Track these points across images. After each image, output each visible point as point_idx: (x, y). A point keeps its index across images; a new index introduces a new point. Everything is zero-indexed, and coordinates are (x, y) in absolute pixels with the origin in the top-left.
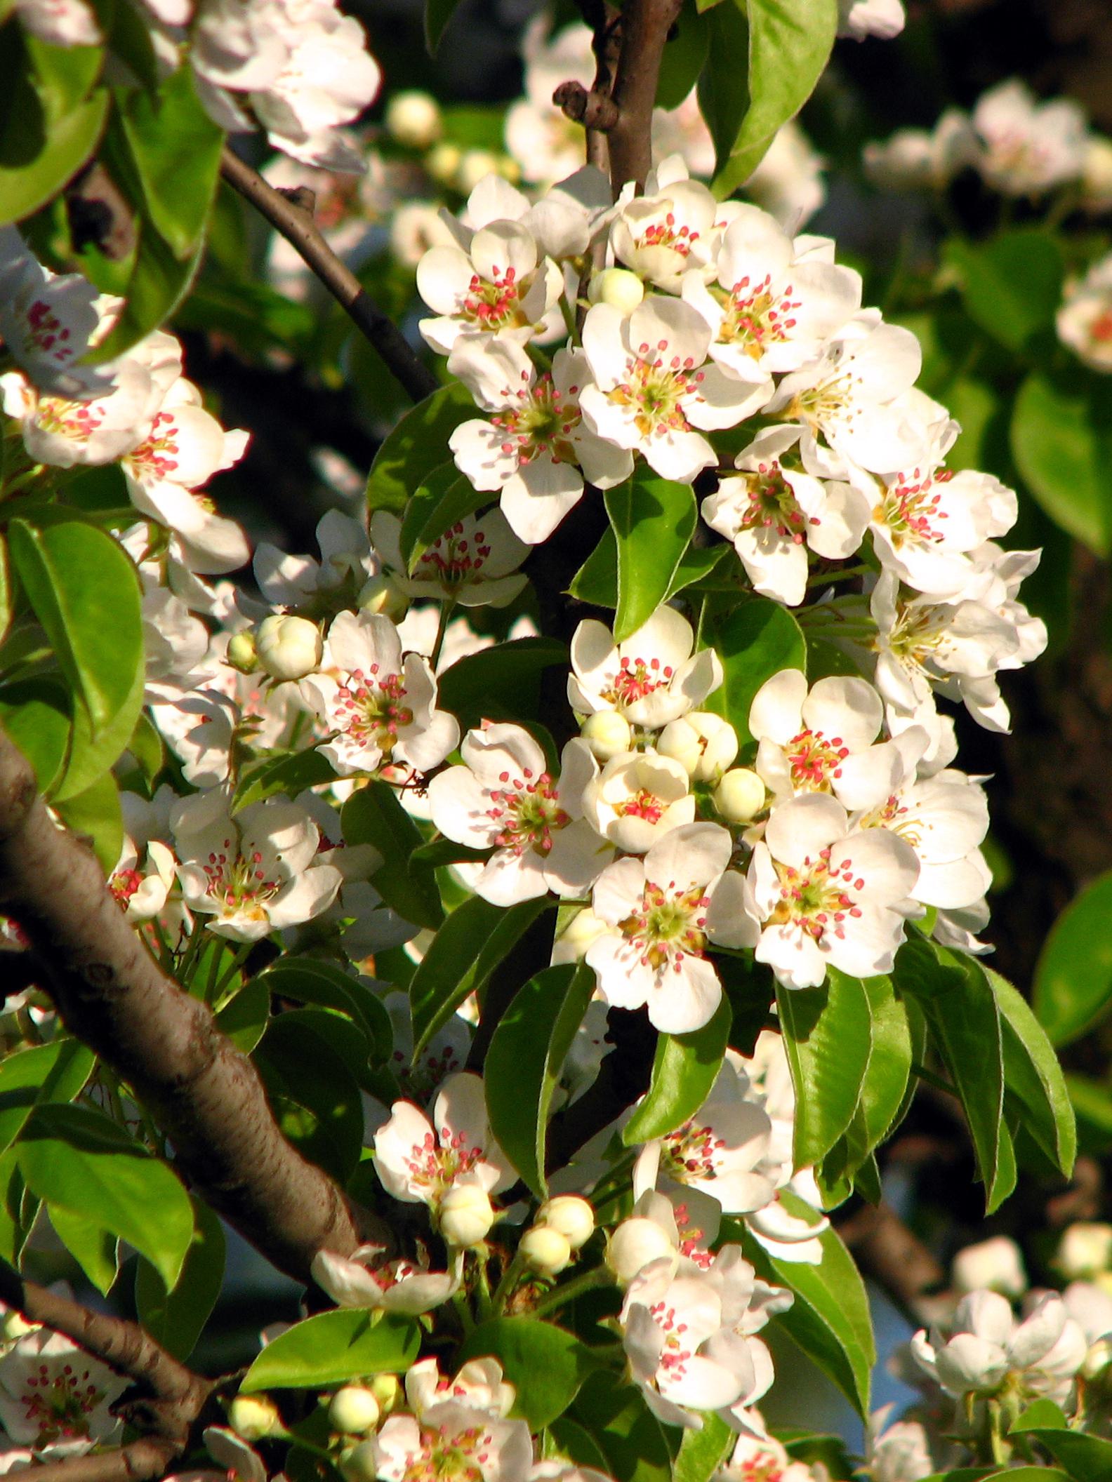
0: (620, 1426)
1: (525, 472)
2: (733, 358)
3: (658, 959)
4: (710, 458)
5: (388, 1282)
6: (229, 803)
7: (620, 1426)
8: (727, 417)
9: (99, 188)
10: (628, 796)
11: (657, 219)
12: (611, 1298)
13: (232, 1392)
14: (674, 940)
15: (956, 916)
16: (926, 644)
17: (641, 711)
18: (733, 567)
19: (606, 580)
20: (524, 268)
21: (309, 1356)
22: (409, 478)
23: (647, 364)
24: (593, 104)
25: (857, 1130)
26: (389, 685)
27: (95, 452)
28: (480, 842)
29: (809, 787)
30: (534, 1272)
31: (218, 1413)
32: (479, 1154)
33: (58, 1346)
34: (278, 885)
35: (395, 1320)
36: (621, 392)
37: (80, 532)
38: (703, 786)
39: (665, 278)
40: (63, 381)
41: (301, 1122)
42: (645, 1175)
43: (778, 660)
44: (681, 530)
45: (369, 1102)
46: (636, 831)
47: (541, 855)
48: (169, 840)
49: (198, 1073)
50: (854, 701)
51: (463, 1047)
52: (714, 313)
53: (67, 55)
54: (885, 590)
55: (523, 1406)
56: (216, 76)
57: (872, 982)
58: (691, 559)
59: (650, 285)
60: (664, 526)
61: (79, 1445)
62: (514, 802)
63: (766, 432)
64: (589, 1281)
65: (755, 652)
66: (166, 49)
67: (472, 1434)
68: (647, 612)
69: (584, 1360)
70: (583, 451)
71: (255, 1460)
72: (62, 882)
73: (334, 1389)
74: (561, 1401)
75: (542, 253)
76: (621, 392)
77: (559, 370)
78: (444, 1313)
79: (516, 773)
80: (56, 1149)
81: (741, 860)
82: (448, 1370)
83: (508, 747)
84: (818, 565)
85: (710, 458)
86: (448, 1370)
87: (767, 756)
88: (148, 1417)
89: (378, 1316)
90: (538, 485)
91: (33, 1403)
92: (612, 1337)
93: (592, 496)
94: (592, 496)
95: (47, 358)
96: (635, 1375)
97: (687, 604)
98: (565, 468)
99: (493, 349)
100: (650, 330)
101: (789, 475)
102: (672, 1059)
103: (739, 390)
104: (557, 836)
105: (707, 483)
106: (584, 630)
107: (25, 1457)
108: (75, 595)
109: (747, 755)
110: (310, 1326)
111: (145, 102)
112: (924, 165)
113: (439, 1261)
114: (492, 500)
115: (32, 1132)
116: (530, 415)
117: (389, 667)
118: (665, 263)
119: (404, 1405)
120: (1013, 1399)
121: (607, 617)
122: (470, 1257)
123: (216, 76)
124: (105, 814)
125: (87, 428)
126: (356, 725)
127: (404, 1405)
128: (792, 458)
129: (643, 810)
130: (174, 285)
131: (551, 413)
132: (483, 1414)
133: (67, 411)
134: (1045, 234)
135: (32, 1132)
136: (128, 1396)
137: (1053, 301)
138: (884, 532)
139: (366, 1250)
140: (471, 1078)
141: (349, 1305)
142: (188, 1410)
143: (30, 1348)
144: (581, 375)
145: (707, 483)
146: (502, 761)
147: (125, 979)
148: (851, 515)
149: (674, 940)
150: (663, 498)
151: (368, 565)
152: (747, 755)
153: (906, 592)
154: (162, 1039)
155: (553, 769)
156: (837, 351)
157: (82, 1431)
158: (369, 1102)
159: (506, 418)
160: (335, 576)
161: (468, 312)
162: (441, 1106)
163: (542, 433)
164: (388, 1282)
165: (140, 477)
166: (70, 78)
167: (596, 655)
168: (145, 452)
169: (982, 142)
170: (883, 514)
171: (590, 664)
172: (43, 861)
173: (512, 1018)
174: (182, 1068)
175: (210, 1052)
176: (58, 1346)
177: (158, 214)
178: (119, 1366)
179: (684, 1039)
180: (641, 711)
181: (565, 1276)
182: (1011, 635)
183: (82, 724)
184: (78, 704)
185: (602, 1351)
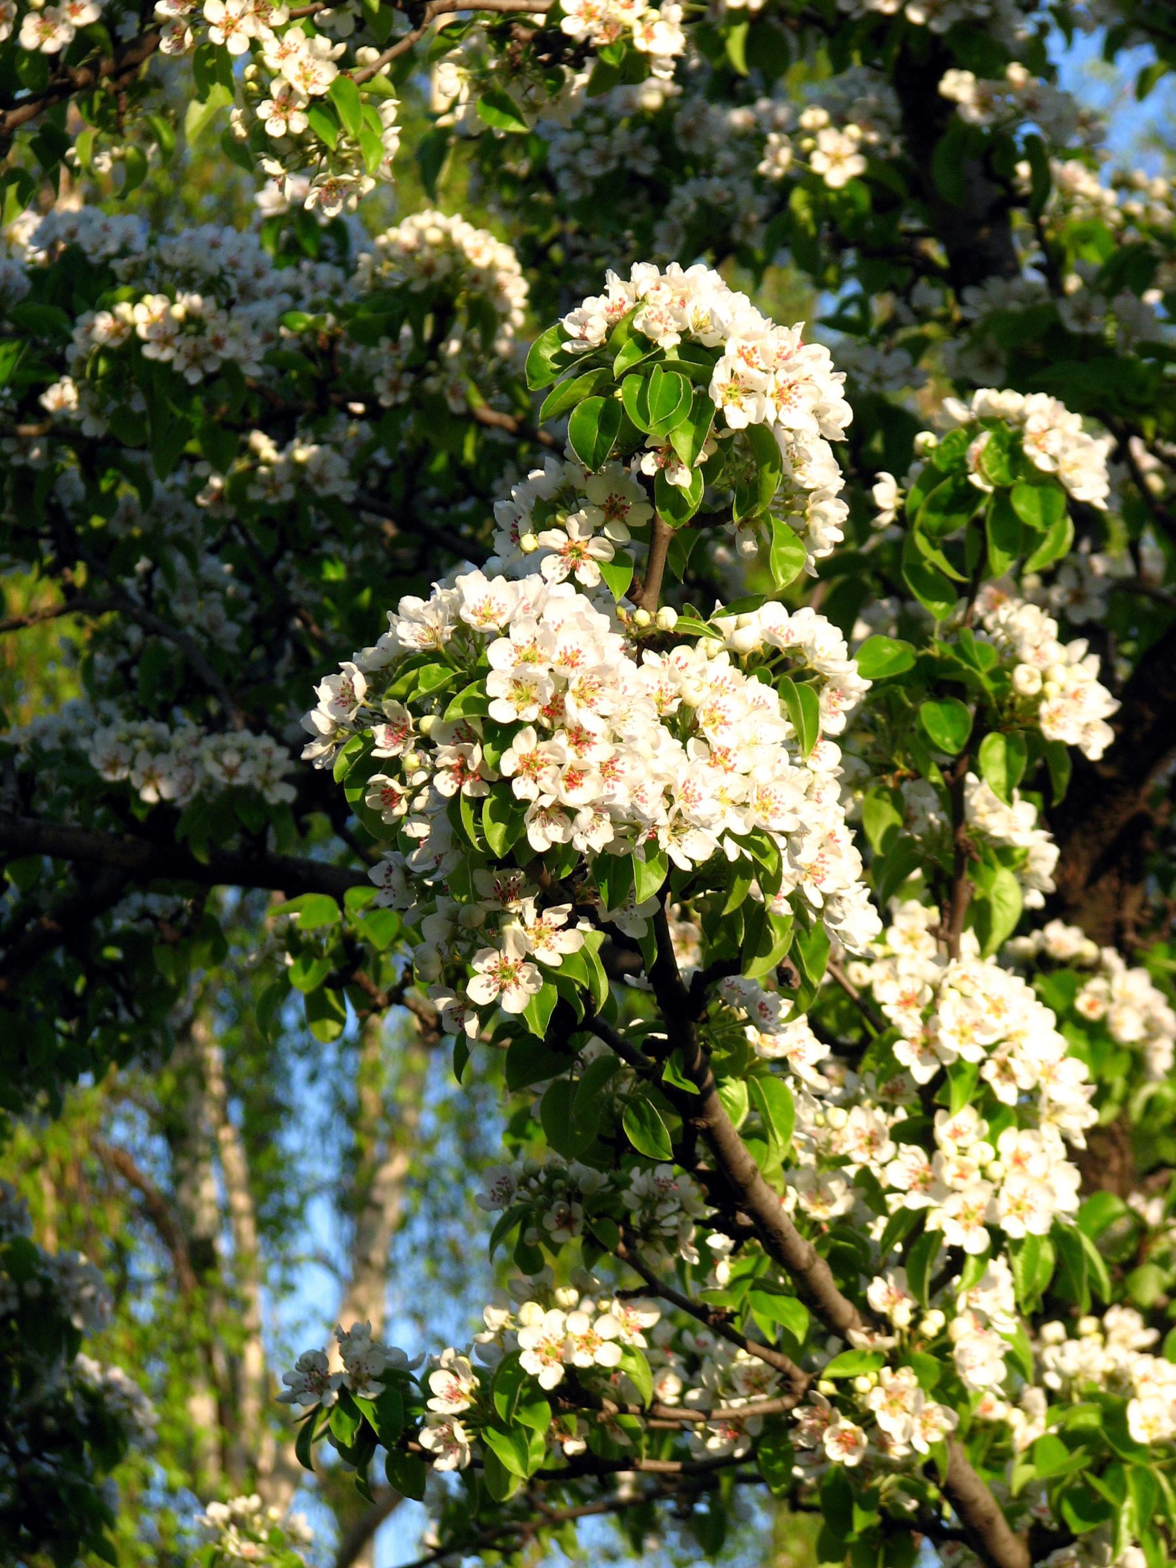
0: (953, 1390)
1: (920, 1059)
2: (990, 1020)
3: (967, 1227)
4: (983, 1054)
5: (872, 1339)
6: (815, 1173)
7: (953, 1390)
8: (990, 1040)
9: (788, 964)
10: (957, 1171)
11: (963, 972)
12: (949, 1346)
13: (818, 1378)
14: (973, 1221)
15: (1068, 1214)
16: (1057, 1118)
17: (961, 1142)
18: (990, 1093)
19: (947, 1096)
20: (918, 989)
21: (845, 1366)
22: (878, 1061)
23: (961, 1022)
24: (941, 932)
25: (1036, 1288)
26: (873, 1133)
27: (779, 1053)
28: (904, 1187)
29: (1017, 1169)
30: (922, 1337)
31: (813, 1386)
32: (905, 1296)
33: (757, 1362)
34: (831, 1201)
35: (877, 1354)
36: (953, 1032)
37: (774, 1081)
38: (983, 1168)
39: (967, 992)
40: (771, 1029)
41: (841, 1284)
42: (960, 1305)
43: (1007, 1124)
44: (973, 1078)
45: (862, 1278)
46: (959, 1184)
47: (926, 1191)
48: (794, 1185)
49: (810, 1267)
50: (1034, 1138)
51: (894, 1259)
52: (985, 1005)
53: (782, 919)
54: (1043, 1100)
55: (921, 1384)
56: (831, 925)
57: (1041, 1237)
58: (977, 1089)
59: (963, 995)
60: (967, 1078)
61: (763, 1397)
62: (916, 1173)
63: (1003, 1045)
64: (943, 1340)
65: (998, 1121)
66: (812, 916)
67: (902, 1393)
68: (962, 1106)
69: (942, 1368)
70: (939, 1051)
71: (827, 1403)
72: (765, 1202)
73: (853, 1378)
74: (933, 1381)
75: (925, 983)
76: (953, 1032)
77: (931, 1024)
78: (893, 1352)
79: (917, 1163)
80: (760, 1294)
81: (996, 1193)
82: (894, 1370)
83: (914, 1154)
84: (1021, 1092)
85: (983, 1054)
86: (894, 1370)
87: (1003, 1157)
88: (789, 1387)
89: (869, 1352)
90: (924, 1062)
91: (747, 1382)
92: (950, 1360)
93: (943, 1068)
94: (943, 1068)
95: (765, 1021)
96: (959, 1373)
97: (975, 1105)
98: (933, 1058)
99: (909, 1016)
100: (963, 1009)
101: (1010, 1060)
102: (971, 1264)
103: (992, 1031)
104: (932, 1186)
105: (982, 1063)
106: (940, 1114)
107: (744, 1401)
108: (771, 1102)
109: (997, 1157)
110: (847, 1356)
111: (805, 934)
112: (1026, 950)
113: (890, 1331)
114: (907, 1069)
115: (753, 1288)
116: (921, 1039)
117: (872, 1126)
118: (967, 987)
119: (879, 1384)
120: (1081, 1380)
121: (947, 1109)
122: (901, 1331)
123: (831, 925)
124: (778, 1177)
125: (775, 1045)
126: (860, 1147)
127: (879, 1384)
128: (1011, 1054)
129: (962, 1176)
130: (812, 997)
131: (928, 1038)
132: (907, 1387)
133: (768, 1038)
134: (1069, 973)
135: (753, 1288)
136: (783, 1380)
137: (1073, 995)
138: (1043, 1080)
139: (865, 1329)
140: (902, 1271)
141: (859, 1348)
142: (803, 1385)
143: (746, 1363)
144: (938, 1026)
145: (982, 1063)
146: (913, 1159)
147: (786, 1235)
148: (1032, 1074)
149: (973, 1221)
150: (966, 1067)
151: (862, 1091)
152: (997, 1157)
153: (1050, 1101)
154: (798, 1256)
155: (930, 1160)
156: (1026, 1018)
157: (764, 1392)
158: (862, 1278)
159: (912, 1040)
160: (851, 1094)
161: (900, 1003)
162: (891, 1278)
163: (926, 1045)
164: (872, 1339)
165: (794, 1063)
166: (783, 928)
167: (945, 1120)
168: (795, 1053)
169: (1047, 940)
170: (1043, 1074)
171: (941, 1124)
172: (759, 1195)
173: (915, 1249)
174: (804, 1265)
175: (814, 1260)
176: (757, 1362)
177: (808, 973)
178: (779, 1369)
179: (977, 1256)
180: (961, 1142)
181: (935, 1338)
182: (1085, 1114)
183: (773, 1147)
184: (771, 1139)
185: (947, 1364)
